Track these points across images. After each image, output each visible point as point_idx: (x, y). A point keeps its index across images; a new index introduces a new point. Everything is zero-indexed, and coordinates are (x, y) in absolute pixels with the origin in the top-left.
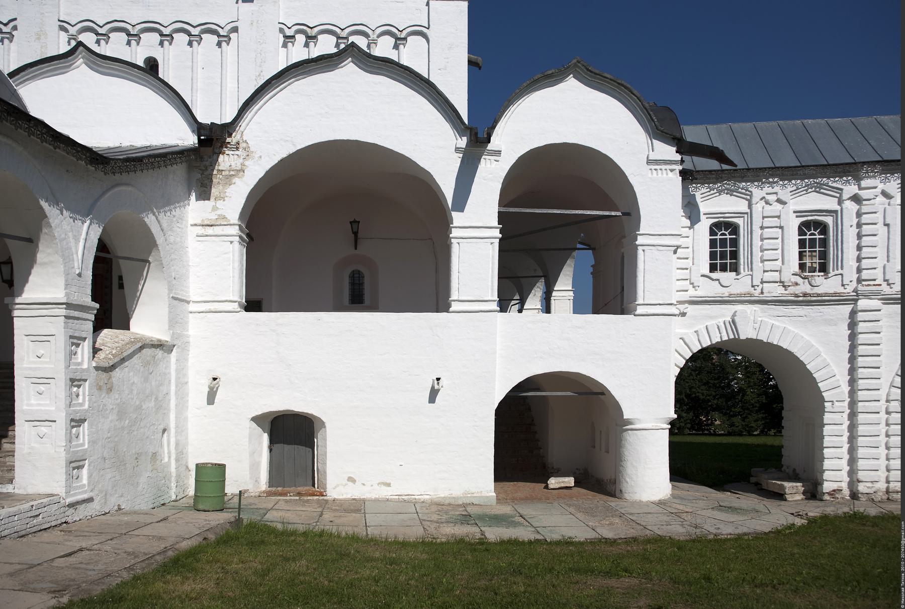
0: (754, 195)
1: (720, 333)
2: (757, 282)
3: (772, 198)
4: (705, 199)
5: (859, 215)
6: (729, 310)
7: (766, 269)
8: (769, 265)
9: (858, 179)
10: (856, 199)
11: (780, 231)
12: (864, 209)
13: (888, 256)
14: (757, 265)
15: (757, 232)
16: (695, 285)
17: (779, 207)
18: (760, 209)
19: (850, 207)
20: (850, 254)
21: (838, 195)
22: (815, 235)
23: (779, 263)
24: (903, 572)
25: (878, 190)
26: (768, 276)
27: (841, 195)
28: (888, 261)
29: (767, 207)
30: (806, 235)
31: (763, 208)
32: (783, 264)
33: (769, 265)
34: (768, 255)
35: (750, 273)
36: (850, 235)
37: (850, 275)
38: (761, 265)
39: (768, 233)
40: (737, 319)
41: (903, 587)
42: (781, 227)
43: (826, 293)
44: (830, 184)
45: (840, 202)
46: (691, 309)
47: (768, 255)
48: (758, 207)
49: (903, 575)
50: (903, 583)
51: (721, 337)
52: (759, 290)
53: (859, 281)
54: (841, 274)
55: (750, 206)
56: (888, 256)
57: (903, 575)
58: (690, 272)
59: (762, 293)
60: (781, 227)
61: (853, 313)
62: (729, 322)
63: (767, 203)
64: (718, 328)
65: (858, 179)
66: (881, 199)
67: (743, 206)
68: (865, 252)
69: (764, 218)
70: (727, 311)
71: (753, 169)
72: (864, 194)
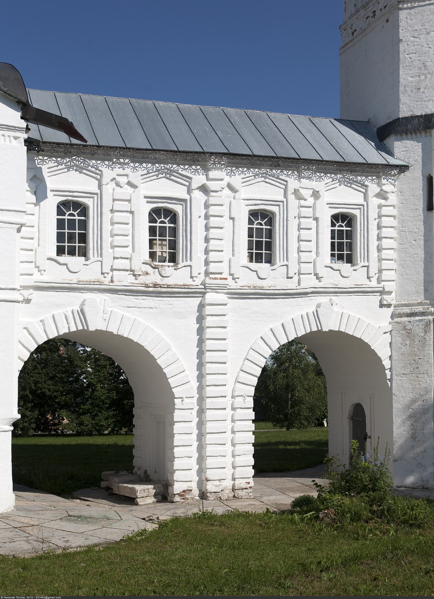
1: (68, 324)
2: (106, 269)
3: (123, 180)
8: (119, 252)
9: (206, 170)
10: (204, 189)
12: (212, 201)
14: (107, 251)
17: (130, 190)
19: (198, 196)
21: (187, 184)
23: (129, 250)
26: (118, 264)
27: (190, 183)
28: (233, 255)
29: (118, 189)
32: (133, 251)
33: (119, 252)
34: (118, 240)
39: (118, 217)
40: (86, 309)
41: (16, 597)
42: (132, 212)
45: (189, 191)
46: (36, 296)
47: (118, 240)
49: (24, 598)
50: (18, 598)
55: (100, 186)
56: (233, 250)
57: (24, 598)
61: (201, 306)
62: (78, 311)
63: (118, 185)
65: (206, 170)
66: (227, 191)
67: (359, 199)
68: (213, 244)
69: (114, 200)
72: (212, 185)
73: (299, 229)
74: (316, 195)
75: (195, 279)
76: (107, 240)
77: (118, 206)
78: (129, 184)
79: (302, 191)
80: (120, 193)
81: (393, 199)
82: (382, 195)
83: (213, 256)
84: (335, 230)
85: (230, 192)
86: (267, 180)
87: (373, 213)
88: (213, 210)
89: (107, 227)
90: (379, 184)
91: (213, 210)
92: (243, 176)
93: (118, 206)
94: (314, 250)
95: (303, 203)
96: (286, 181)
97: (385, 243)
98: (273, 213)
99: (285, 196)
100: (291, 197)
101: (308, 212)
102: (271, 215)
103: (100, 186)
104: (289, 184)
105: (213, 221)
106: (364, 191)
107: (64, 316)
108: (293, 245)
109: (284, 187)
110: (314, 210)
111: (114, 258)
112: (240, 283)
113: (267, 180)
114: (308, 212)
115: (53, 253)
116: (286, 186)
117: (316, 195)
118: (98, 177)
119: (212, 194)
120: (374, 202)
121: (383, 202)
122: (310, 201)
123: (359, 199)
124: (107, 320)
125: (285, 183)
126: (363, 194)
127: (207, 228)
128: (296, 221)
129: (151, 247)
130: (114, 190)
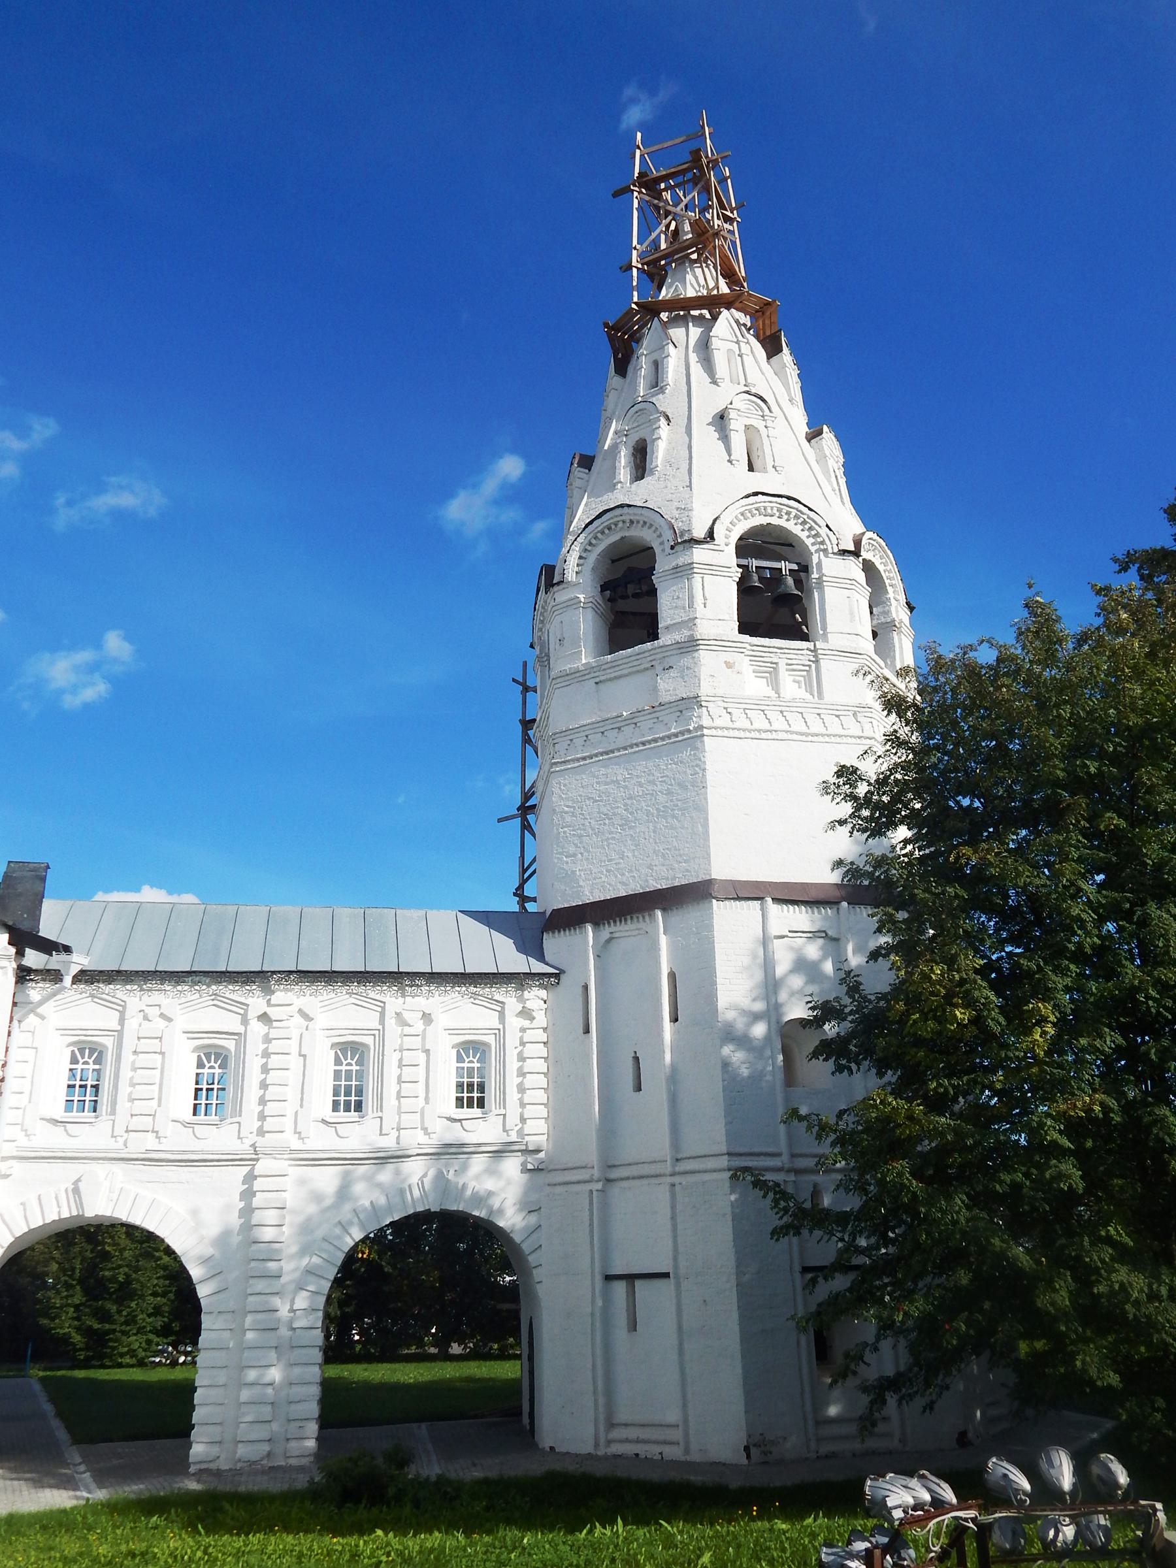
0: (128, 1006)
1: (59, 1207)
2: (120, 1130)
3: (153, 1012)
4: (326, 1009)
5: (267, 1039)
6: (72, 1171)
7: (134, 1113)
8: (139, 1107)
9: (268, 991)
10: (264, 1018)
11: (159, 1057)
12: (274, 1033)
13: (302, 1099)
14: (123, 1105)
15: (127, 1057)
16: (29, 1133)
17: (162, 1023)
18: (137, 1027)
19: (257, 1029)
20: (252, 1093)
21: (242, 1012)
22: (351, 1065)
23: (154, 1103)
24: (1126, 1507)
25: (294, 1009)
26: (136, 1123)
27: (246, 1011)
28: (301, 1106)
29: (146, 1024)
30: (342, 1065)
31: (140, 1025)
32: (159, 1105)
33: (139, 1107)
34: (140, 1091)
35: (380, 1114)
36: (253, 1065)
37: (249, 1120)
38: (128, 1105)
39: (142, 1060)
40: (81, 1185)
42: (162, 1053)
43: (451, 1145)
44: (227, 995)
45: (245, 1021)
46: (16, 1167)
47: (140, 1091)
48: (133, 1023)
51: (59, 1212)
52: (121, 1140)
53: (261, 1132)
54: (239, 1123)
55: (122, 1021)
56: (302, 1099)
58: (24, 1115)
59: (125, 1145)
60: (162, 1053)
61: (250, 1178)
62: (66, 1190)
63: (146, 1018)
64: (57, 1198)
65: (268, 991)
66: (298, 1019)
67: (370, 1020)
68: (272, 1093)
69: (139, 1038)
70: (67, 1173)
71: (161, 972)
72: (273, 1013)
73: (400, 1066)
74: (427, 1018)
75: (32, 1137)
76: (124, 1090)
77: (144, 1045)
78: (162, 1016)
79: (406, 1015)
80: (148, 1029)
81: (541, 1019)
82: (526, 1014)
83: (270, 1108)
84: (463, 1068)
85: (301, 1020)
86: (476, 1002)
87: (512, 1041)
88: (274, 1046)
89: (126, 1073)
90: (521, 999)
91: (274, 1046)
92: (183, 1000)
93: (144, 1045)
94: (422, 1095)
95: (407, 1030)
96: (384, 1003)
97: (530, 1081)
98: (366, 1046)
99: (382, 1020)
100: (390, 1022)
101: (416, 1042)
102: (482, 1048)
103: (122, 1021)
104: (387, 1006)
105: (274, 1061)
106: (499, 1009)
107: (54, 1196)
108: (391, 1088)
109: (379, 1009)
110: (424, 1039)
111: (132, 1115)
112: (310, 1144)
113: (476, 1002)
114: (416, 1042)
115: (187, 1114)
116: (383, 1008)
117: (427, 1018)
118: (120, 1008)
119: (275, 1024)
120: (514, 1023)
121: (527, 1023)
122: (419, 1026)
123: (491, 1019)
124: (115, 1201)
125: (382, 1005)
126: (118, 1014)
127: (265, 1069)
128: (397, 1055)
129: (196, 1098)
130: (140, 1025)
